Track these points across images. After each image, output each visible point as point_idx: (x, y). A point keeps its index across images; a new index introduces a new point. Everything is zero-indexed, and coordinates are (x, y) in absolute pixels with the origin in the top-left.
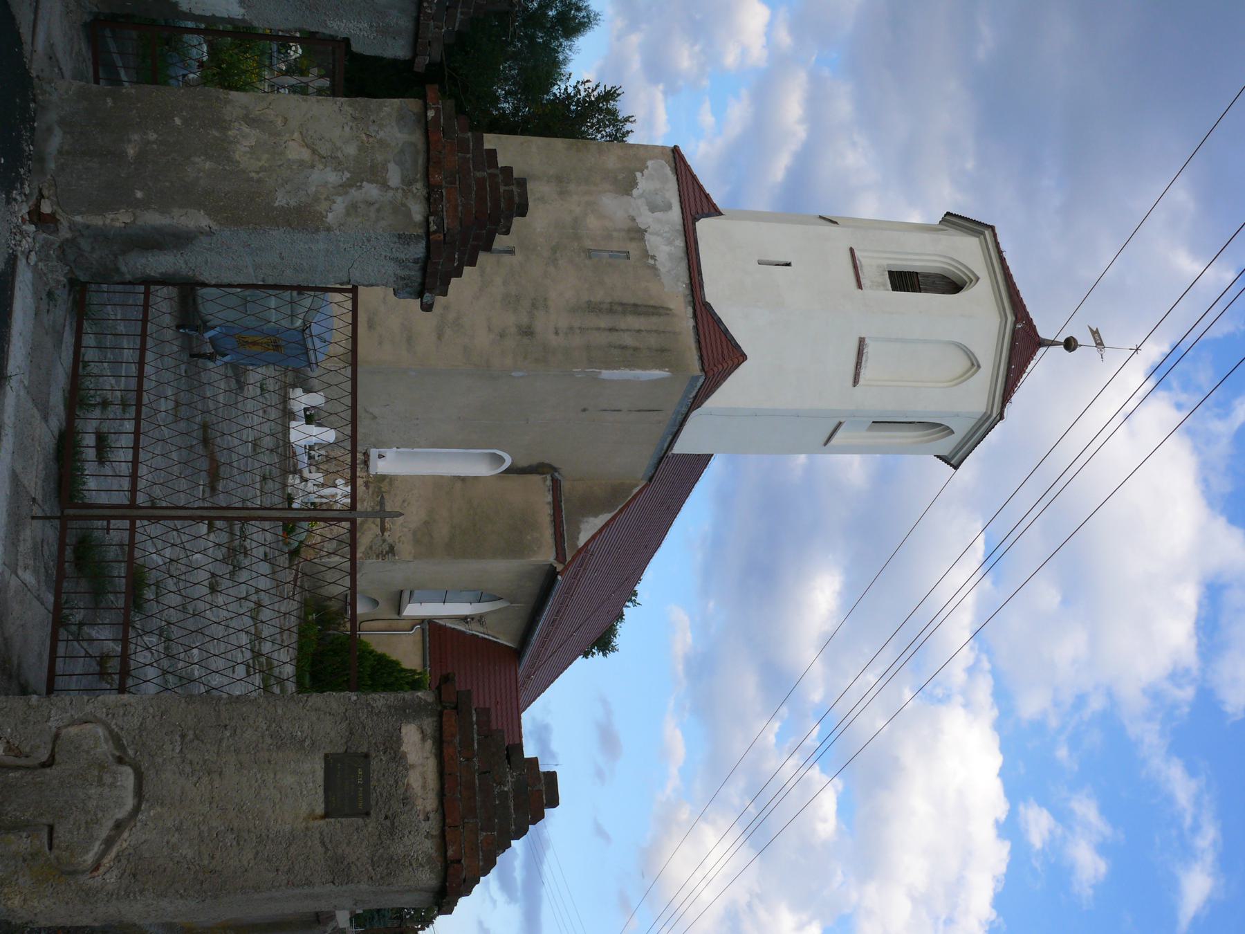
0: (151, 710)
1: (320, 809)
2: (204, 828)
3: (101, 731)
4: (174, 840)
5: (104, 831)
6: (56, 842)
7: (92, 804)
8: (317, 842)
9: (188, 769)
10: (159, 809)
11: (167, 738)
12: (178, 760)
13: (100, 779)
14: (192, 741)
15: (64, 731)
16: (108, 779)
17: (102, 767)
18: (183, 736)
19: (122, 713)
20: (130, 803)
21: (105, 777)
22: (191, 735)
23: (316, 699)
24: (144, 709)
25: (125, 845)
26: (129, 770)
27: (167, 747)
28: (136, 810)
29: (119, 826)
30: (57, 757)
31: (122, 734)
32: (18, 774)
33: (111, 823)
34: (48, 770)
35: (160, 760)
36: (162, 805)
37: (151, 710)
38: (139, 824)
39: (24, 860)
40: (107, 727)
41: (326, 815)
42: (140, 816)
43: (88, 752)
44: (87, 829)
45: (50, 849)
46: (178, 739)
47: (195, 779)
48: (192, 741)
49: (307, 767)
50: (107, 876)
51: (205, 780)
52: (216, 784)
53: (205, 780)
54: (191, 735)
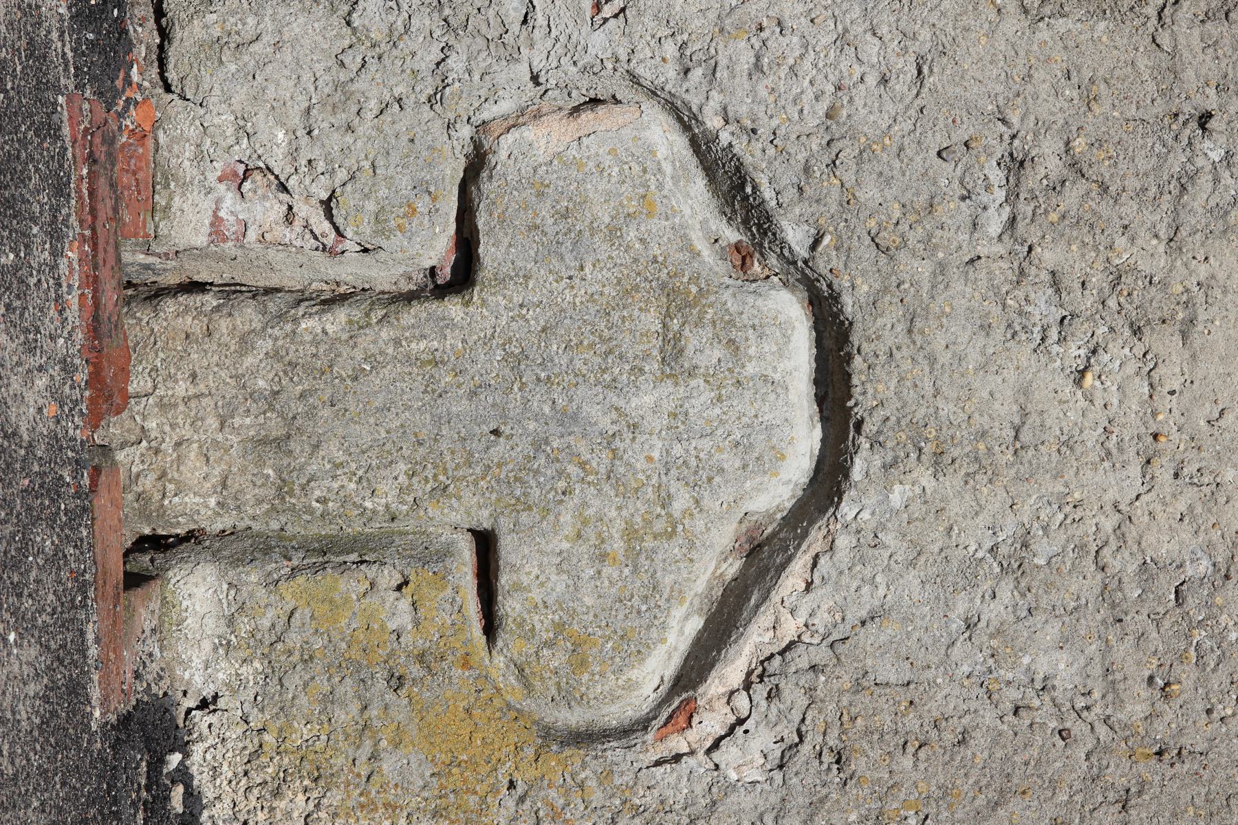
0: (871, 49)
2: (1123, 564)
4: (994, 612)
5: (711, 565)
9: (1043, 308)
11: (946, 172)
12: (1003, 271)
13: (672, 352)
14: (1057, 187)
15: (504, 148)
16: (703, 349)
18: (1016, 164)
19: (746, 60)
20: (804, 441)
21: (692, 340)
23: (121, 575)
25: (790, 628)
26: (789, 310)
27: (954, 212)
28: (828, 482)
29: (764, 556)
30: (488, 251)
31: (751, 154)
32: (336, 321)
33: (725, 535)
34: (453, 307)
35: (924, 269)
36: (939, 462)
37: (871, 49)
39: (397, 682)
42: (847, 509)
43: (614, 233)
44: (633, 556)
46: (996, 176)
47: (1075, 351)
49: (204, 727)
50: (728, 754)
51: (1119, 355)
52: (1170, 376)
53: (1119, 355)
54: (1050, 163)
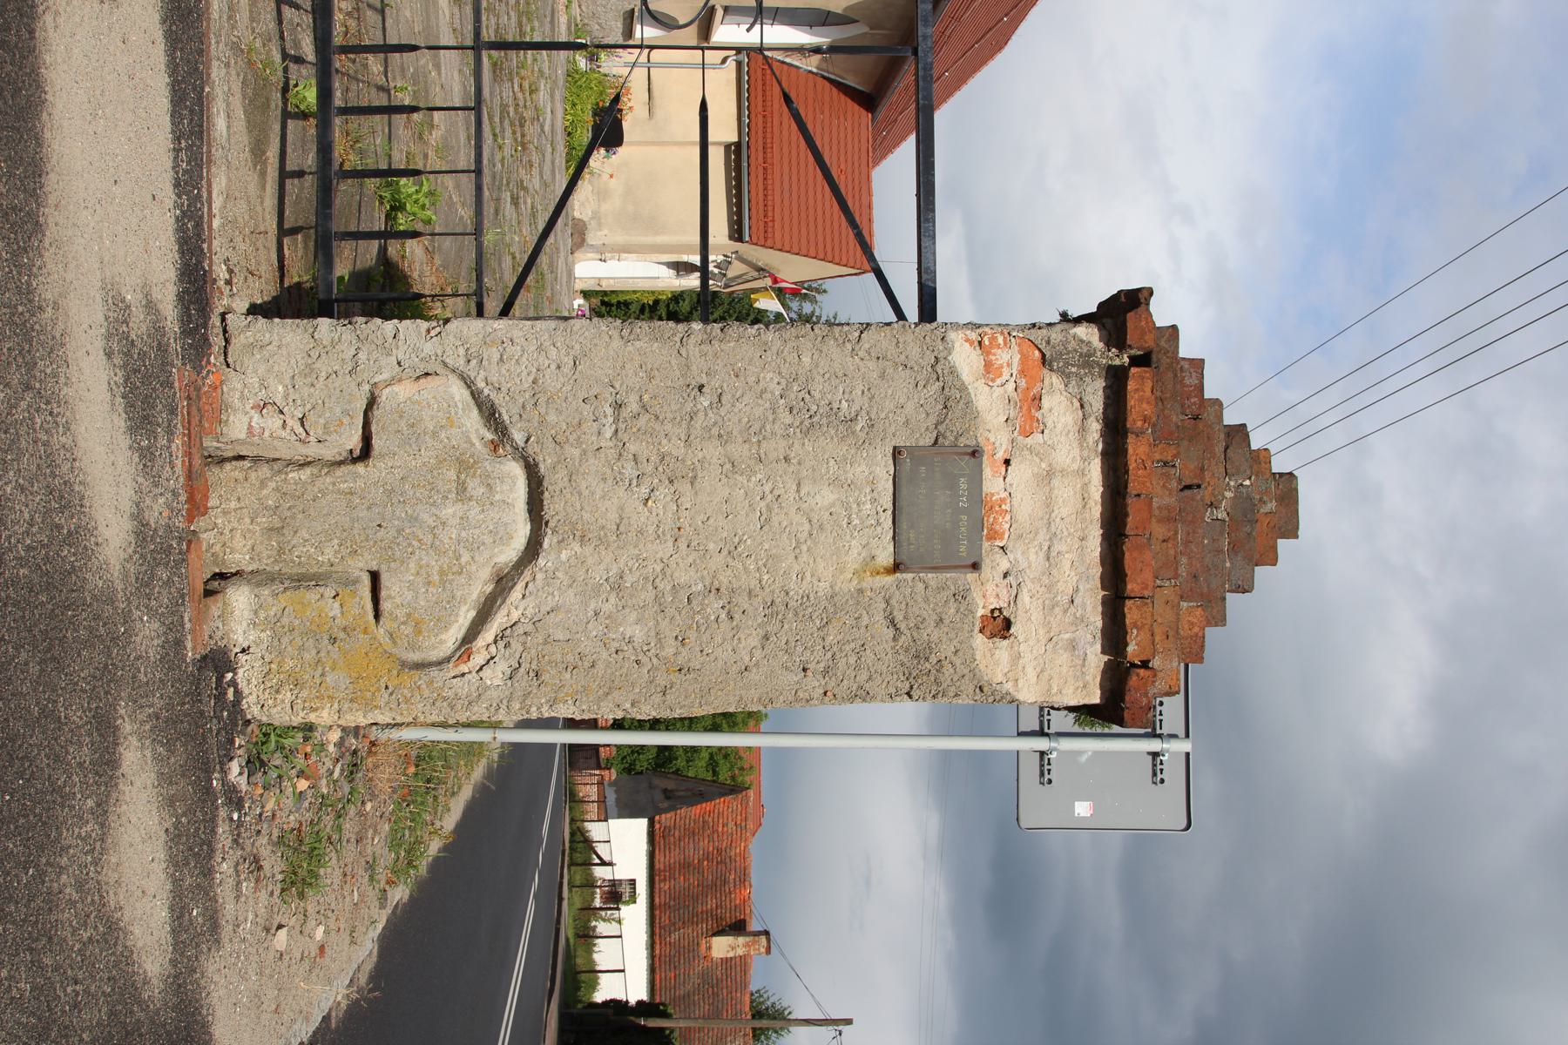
1: (885, 557)
3: (459, 392)
4: (607, 608)
5: (480, 586)
6: (386, 606)
7: (448, 536)
8: (879, 617)
9: (630, 471)
10: (576, 547)
13: (462, 488)
14: (636, 416)
15: (384, 395)
16: (475, 488)
17: (465, 466)
18: (618, 406)
19: (496, 356)
20: (523, 530)
22: (633, 406)
24: (540, 348)
25: (515, 615)
26: (516, 471)
28: (533, 548)
29: (503, 583)
30: (375, 442)
31: (498, 399)
32: (305, 474)
35: (576, 452)
37: (553, 353)
38: (540, 576)
39: (333, 640)
40: (469, 384)
41: (896, 567)
42: (541, 561)
43: (435, 434)
44: (443, 583)
45: (377, 616)
46: (609, 411)
47: (644, 490)
48: (636, 416)
54: (633, 406)
